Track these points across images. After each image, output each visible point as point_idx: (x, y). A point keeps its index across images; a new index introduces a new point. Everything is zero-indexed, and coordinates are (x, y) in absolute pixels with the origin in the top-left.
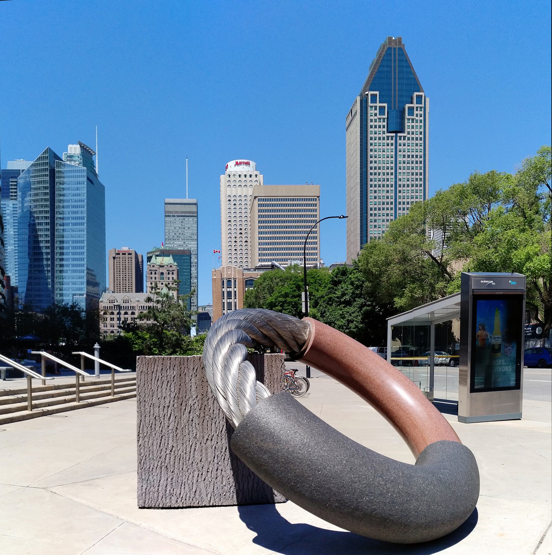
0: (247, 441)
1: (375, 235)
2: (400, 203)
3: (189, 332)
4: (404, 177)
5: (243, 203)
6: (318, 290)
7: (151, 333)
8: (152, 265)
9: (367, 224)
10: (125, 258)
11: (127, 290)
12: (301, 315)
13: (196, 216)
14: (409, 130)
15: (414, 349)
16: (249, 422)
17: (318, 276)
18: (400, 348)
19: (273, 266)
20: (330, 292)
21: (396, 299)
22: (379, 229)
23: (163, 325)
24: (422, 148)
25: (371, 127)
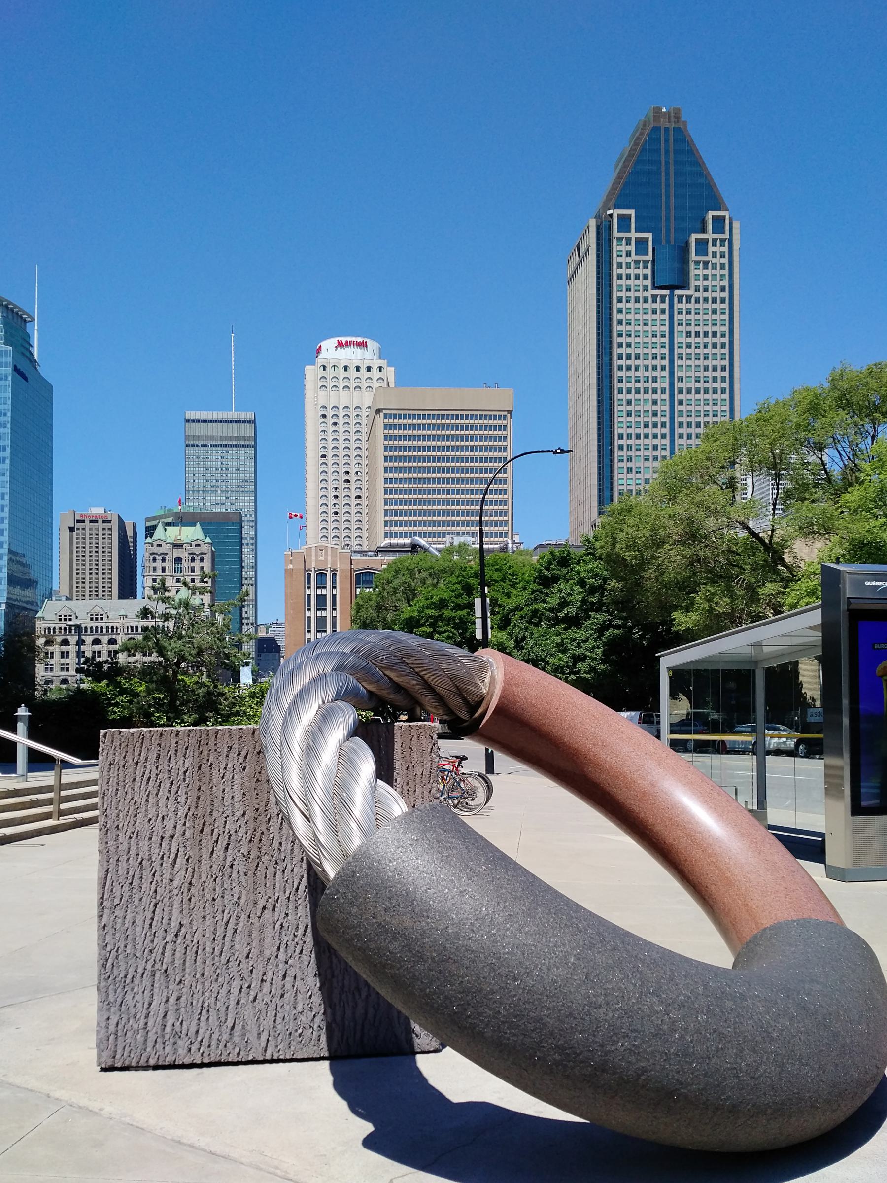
0: (354, 910)
1: (630, 488)
2: (681, 425)
3: (237, 679)
4: (689, 374)
5: (353, 421)
6: (508, 596)
7: (151, 681)
8: (155, 544)
9: (611, 466)
10: (97, 529)
11: (100, 593)
12: (473, 645)
13: (252, 446)
14: (697, 283)
15: (715, 716)
16: (356, 869)
17: (510, 568)
18: (688, 714)
19: (414, 547)
20: (536, 599)
21: (676, 615)
22: (638, 476)
23: (178, 664)
24: (726, 317)
25: (620, 277)
